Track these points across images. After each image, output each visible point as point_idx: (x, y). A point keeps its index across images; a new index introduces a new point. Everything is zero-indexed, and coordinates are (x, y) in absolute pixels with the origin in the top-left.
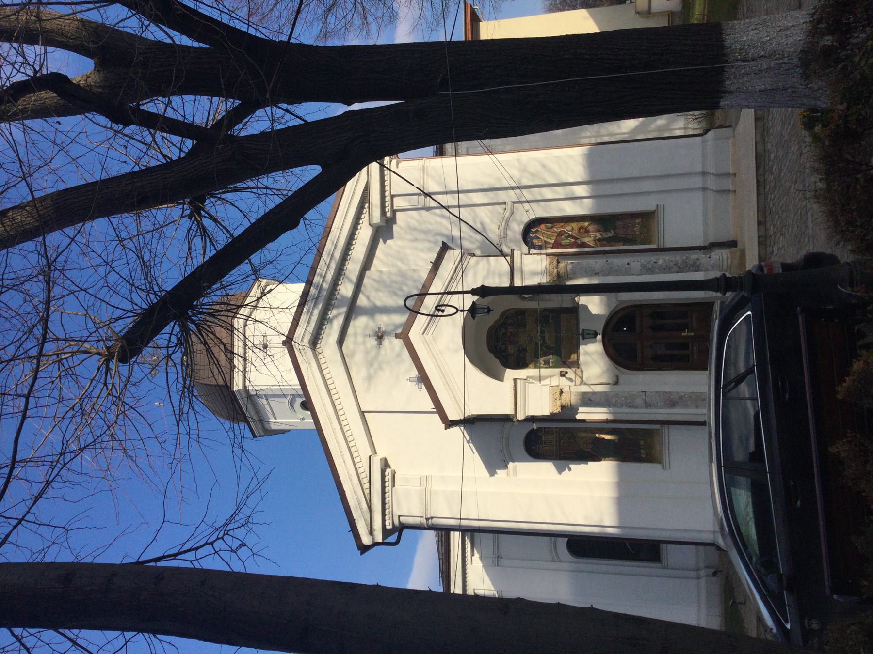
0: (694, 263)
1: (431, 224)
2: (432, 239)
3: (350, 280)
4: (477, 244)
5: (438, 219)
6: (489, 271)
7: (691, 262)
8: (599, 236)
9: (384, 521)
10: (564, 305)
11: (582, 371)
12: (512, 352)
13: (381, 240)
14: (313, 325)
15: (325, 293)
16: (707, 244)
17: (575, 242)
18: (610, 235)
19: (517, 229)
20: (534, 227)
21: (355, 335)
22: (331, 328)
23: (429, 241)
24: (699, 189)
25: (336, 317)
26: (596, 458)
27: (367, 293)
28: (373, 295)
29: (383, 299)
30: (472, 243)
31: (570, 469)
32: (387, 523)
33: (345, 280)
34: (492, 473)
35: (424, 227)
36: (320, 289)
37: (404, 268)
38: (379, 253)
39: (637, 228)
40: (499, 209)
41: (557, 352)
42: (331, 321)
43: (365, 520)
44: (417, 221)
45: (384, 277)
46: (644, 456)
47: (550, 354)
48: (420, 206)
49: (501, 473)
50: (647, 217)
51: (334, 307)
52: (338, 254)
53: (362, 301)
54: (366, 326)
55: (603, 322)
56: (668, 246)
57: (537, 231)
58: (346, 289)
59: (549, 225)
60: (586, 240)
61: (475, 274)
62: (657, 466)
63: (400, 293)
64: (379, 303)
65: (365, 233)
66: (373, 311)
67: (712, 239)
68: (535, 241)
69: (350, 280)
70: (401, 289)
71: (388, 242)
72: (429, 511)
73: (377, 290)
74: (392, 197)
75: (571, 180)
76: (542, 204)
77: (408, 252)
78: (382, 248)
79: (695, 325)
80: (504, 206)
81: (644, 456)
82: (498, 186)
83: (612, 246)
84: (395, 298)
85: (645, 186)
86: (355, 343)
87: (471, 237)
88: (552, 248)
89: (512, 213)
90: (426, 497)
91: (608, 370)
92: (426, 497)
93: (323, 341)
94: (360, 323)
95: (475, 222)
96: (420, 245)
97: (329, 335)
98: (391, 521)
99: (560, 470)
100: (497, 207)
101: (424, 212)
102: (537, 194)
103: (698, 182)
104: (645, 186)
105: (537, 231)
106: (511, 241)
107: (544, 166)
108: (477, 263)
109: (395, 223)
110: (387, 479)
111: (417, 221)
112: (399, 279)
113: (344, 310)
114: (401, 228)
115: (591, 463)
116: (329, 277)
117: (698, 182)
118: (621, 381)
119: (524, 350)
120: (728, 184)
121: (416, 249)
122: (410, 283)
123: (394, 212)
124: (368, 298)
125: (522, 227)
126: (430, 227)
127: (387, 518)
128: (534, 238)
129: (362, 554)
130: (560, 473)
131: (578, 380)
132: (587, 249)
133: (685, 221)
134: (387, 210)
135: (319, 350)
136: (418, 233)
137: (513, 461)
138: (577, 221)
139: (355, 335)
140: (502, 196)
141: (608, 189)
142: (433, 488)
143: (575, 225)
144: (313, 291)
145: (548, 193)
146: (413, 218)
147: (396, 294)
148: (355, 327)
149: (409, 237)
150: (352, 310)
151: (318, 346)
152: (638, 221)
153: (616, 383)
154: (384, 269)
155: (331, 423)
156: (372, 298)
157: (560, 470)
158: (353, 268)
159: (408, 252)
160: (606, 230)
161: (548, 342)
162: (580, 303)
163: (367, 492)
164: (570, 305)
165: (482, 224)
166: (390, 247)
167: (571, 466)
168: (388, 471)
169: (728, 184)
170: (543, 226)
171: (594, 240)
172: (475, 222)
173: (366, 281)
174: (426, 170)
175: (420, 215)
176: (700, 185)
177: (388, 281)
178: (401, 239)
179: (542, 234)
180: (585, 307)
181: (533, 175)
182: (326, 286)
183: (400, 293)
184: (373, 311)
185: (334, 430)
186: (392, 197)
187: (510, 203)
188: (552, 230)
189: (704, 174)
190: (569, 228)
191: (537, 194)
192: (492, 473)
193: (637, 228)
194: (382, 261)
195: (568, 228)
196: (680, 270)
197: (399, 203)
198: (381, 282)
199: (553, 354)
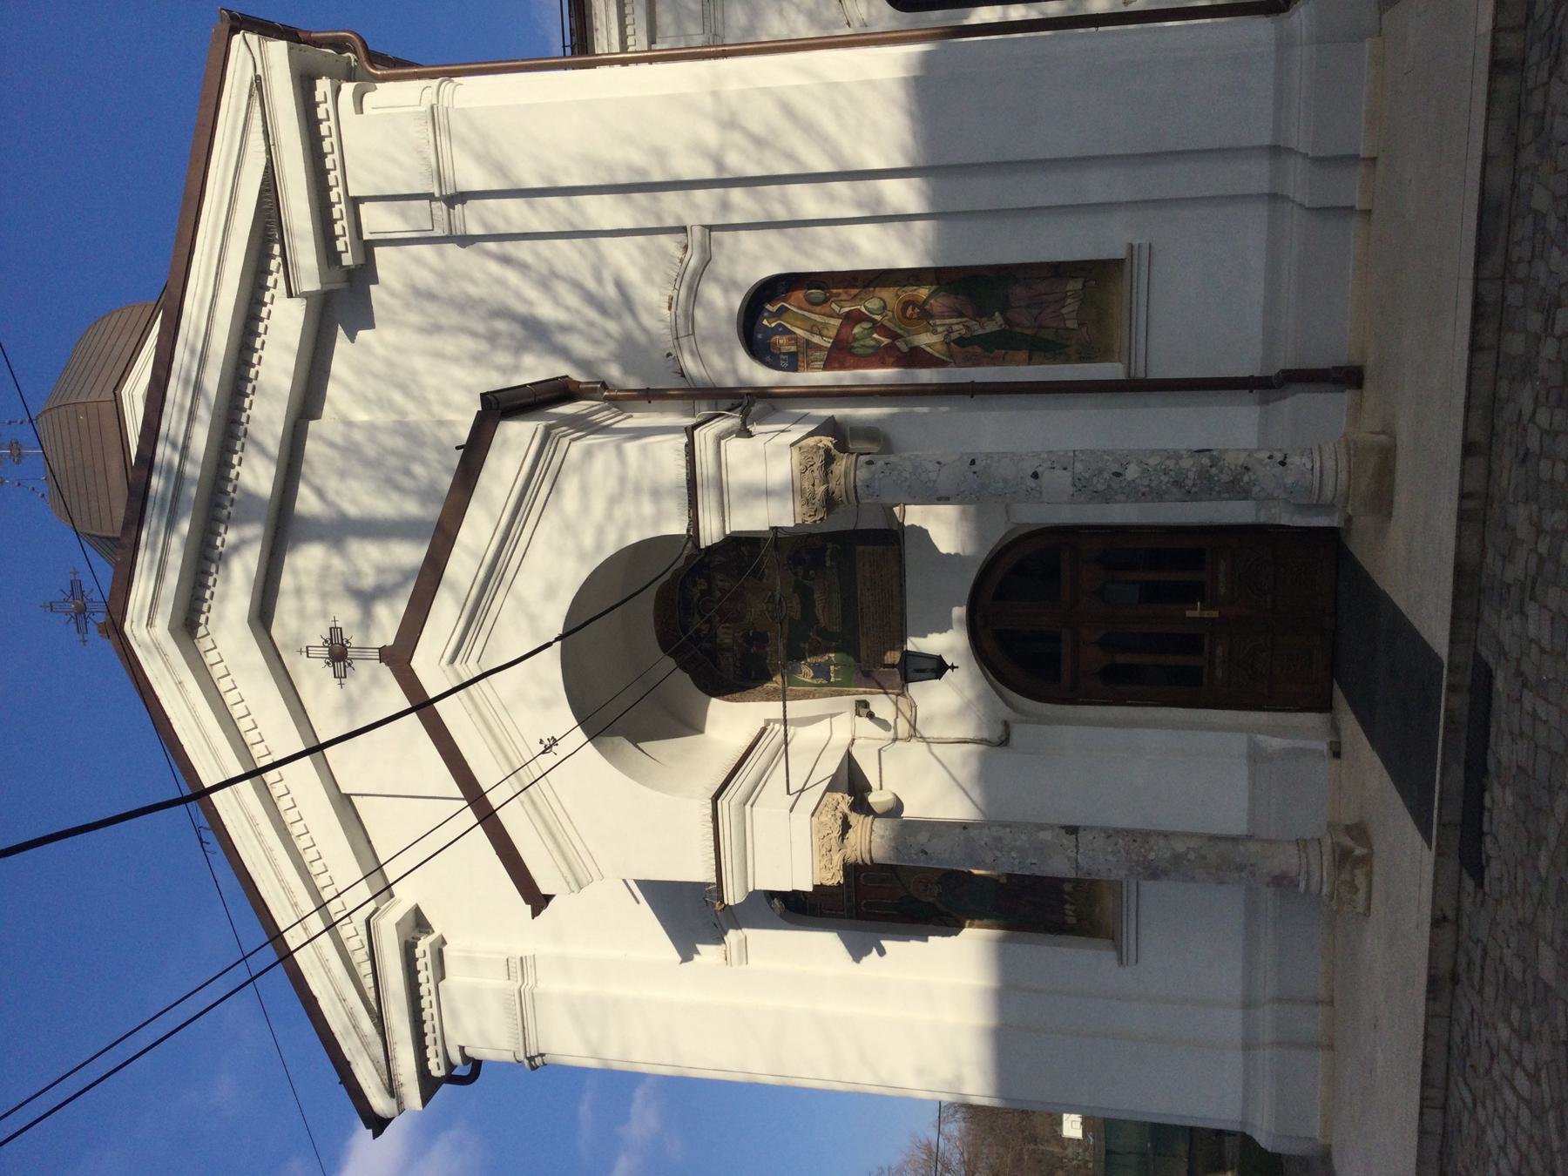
0: (1234, 482)
3: (262, 450)
4: (611, 346)
5: (494, 268)
6: (622, 480)
7: (1225, 478)
8: (959, 329)
9: (422, 1061)
10: (865, 525)
11: (913, 706)
13: (341, 331)
14: (172, 579)
16: (1273, 372)
18: (993, 325)
19: (722, 302)
21: (299, 592)
22: (227, 579)
23: (474, 334)
27: (317, 482)
29: (361, 498)
30: (596, 342)
31: (882, 952)
32: (432, 1065)
33: (249, 448)
34: (687, 954)
35: (454, 289)
36: (179, 479)
37: (415, 414)
38: (337, 366)
40: (669, 243)
41: (847, 644)
42: (223, 559)
43: (374, 1061)
44: (433, 270)
45: (358, 436)
46: (1072, 920)
47: (828, 650)
48: (438, 232)
49: (708, 954)
50: (1099, 275)
51: (229, 521)
52: (212, 380)
53: (307, 502)
54: (325, 570)
55: (972, 575)
56: (1156, 373)
57: (783, 310)
58: (256, 475)
59: (816, 293)
60: (925, 340)
61: (585, 490)
62: (1108, 957)
63: (406, 482)
64: (352, 510)
65: (285, 321)
66: (340, 530)
67: (1287, 359)
69: (262, 450)
70: (408, 473)
71: (362, 334)
72: (532, 1039)
73: (342, 475)
74: (354, 203)
76: (791, 231)
77: (420, 363)
78: (345, 354)
79: (1223, 590)
80: (681, 237)
81: (1072, 920)
82: (657, 176)
84: (395, 496)
85: (1096, 185)
86: (301, 614)
87: (591, 324)
88: (827, 366)
89: (706, 261)
90: (522, 1008)
91: (979, 697)
92: (522, 1008)
94: (306, 561)
95: (599, 280)
96: (450, 344)
97: (223, 598)
99: (858, 953)
101: (452, 249)
102: (775, 203)
103: (1257, 176)
104: (1096, 185)
105: (783, 310)
106: (705, 339)
107: (788, 111)
108: (588, 453)
109: (375, 281)
110: (420, 965)
111: (433, 270)
112: (399, 443)
113: (255, 531)
114: (392, 294)
116: (200, 440)
117: (1257, 176)
118: (1015, 737)
119: (761, 639)
120: (1350, 189)
121: (439, 355)
122: (431, 455)
124: (320, 493)
125: (737, 301)
126: (474, 291)
127: (430, 1053)
128: (775, 331)
129: (376, 1135)
131: (903, 728)
132: (926, 376)
133: (1208, 294)
134: (340, 246)
136: (444, 307)
137: (738, 927)
138: (896, 283)
140: (673, 206)
142: (542, 986)
143: (888, 294)
144: (157, 483)
145: (807, 200)
146: (419, 261)
147: (399, 489)
148: (295, 572)
149: (414, 318)
150: (283, 529)
151: (201, 631)
152: (1074, 285)
153: (1004, 741)
154: (361, 416)
155: (258, 835)
156: (331, 496)
157: (858, 953)
158: (267, 413)
159: (420, 363)
160: (981, 313)
161: (823, 621)
163: (371, 995)
164: (880, 525)
165: (620, 285)
166: (367, 349)
167: (884, 943)
168: (424, 945)
169: (1350, 189)
170: (799, 295)
173: (311, 446)
174: (442, 119)
175: (442, 256)
176: (1265, 188)
177: (371, 451)
178: (399, 324)
179: (797, 322)
180: (922, 534)
181: (759, 142)
182: (193, 470)
183: (406, 482)
184: (340, 530)
185: (268, 853)
186: (354, 203)
187: (697, 234)
188: (825, 309)
189: (1276, 151)
190: (874, 304)
191: (775, 203)
192: (687, 954)
193: (1071, 306)
194: (348, 387)
195: (871, 305)
197: (375, 220)
198: (350, 450)
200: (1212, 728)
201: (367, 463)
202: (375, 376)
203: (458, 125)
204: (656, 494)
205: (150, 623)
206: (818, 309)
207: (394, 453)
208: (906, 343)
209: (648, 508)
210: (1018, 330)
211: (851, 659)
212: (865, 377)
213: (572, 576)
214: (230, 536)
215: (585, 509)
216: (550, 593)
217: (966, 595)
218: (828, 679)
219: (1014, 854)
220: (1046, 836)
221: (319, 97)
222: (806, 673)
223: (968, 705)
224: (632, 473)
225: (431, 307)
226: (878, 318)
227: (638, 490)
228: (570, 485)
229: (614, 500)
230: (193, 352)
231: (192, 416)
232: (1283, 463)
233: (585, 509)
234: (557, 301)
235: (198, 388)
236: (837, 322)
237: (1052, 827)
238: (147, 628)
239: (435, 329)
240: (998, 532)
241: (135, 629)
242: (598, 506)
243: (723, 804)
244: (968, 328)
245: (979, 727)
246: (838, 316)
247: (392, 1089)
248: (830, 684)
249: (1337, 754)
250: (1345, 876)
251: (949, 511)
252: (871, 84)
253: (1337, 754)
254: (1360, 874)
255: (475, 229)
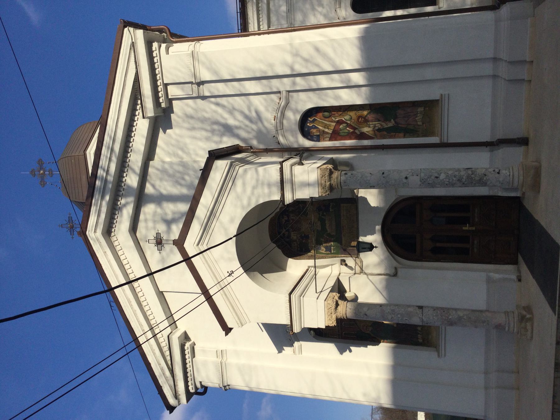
1: (206, 112)
2: (209, 128)
3: (134, 171)
4: (254, 134)
5: (213, 107)
6: (257, 180)
7: (477, 178)
8: (378, 125)
9: (187, 386)
11: (362, 262)
12: (295, 238)
13: (161, 130)
14: (103, 216)
15: (110, 186)
16: (494, 140)
17: (353, 133)
18: (391, 124)
19: (293, 117)
20: (310, 117)
21: (146, 220)
22: (122, 216)
23: (206, 130)
24: (489, 76)
25: (125, 205)
26: (375, 342)
27: (152, 182)
28: (158, 183)
29: (167, 187)
30: (248, 132)
31: (350, 351)
32: (190, 388)
33: (130, 171)
34: (280, 350)
35: (199, 115)
37: (186, 159)
38: (160, 142)
39: (419, 117)
41: (338, 240)
42: (120, 209)
44: (192, 108)
45: (167, 166)
46: (421, 341)
47: (331, 241)
48: (194, 95)
49: (287, 350)
50: (430, 106)
53: (149, 189)
54: (155, 213)
55: (383, 214)
56: (451, 141)
57: (315, 120)
58: (132, 180)
61: (244, 184)
63: (183, 182)
64: (164, 192)
65: (142, 127)
66: (160, 199)
67: (500, 135)
68: (314, 131)
69: (134, 171)
70: (183, 179)
71: (168, 131)
72: (225, 379)
74: (166, 85)
75: (348, 67)
77: (188, 141)
78: (162, 138)
79: (477, 220)
80: (279, 95)
81: (421, 341)
82: (270, 74)
83: (391, 137)
84: (179, 187)
85: (429, 73)
86: (147, 228)
87: (247, 126)
89: (287, 103)
92: (222, 368)
93: (116, 229)
94: (148, 210)
95: (250, 111)
96: (198, 134)
97: (120, 222)
98: (193, 386)
99: (342, 351)
100: (273, 96)
101: (199, 101)
102: (312, 82)
103: (488, 69)
104: (429, 73)
105: (315, 120)
107: (317, 50)
109: (173, 112)
111: (192, 108)
112: (180, 169)
113: (131, 199)
114: (178, 117)
115: (370, 347)
116: (113, 168)
117: (488, 69)
119: (307, 237)
121: (194, 138)
122: (191, 173)
123: (170, 101)
124: (153, 186)
125: (298, 117)
126: (206, 115)
127: (190, 384)
128: (312, 128)
129: (170, 413)
130: (341, 353)
131: (358, 269)
132: (366, 142)
133: (470, 112)
134: (161, 100)
135: (114, 239)
136: (196, 121)
137: (298, 341)
138: (356, 110)
139: (146, 220)
140: (276, 84)
141: (388, 76)
142: (229, 361)
143: (352, 114)
144: (98, 183)
145: (324, 81)
147: (181, 185)
148: (145, 214)
149: (186, 125)
150: (141, 197)
151: (113, 234)
152: (421, 109)
153: (395, 275)
154: (168, 159)
156: (157, 187)
157: (342, 351)
158: (136, 159)
159: (188, 141)
160: (386, 120)
161: (329, 231)
162: (359, 196)
163: (169, 363)
164: (350, 196)
165: (257, 112)
166: (170, 136)
167: (351, 348)
168: (188, 345)
170: (320, 115)
171: (374, 131)
172: (250, 111)
173: (150, 170)
174: (195, 55)
175: (195, 103)
176: (491, 73)
177: (171, 171)
178: (181, 127)
180: (365, 199)
181: (306, 60)
182: (110, 178)
183: (183, 182)
184: (160, 199)
186: (166, 85)
187: (284, 93)
189: (495, 60)
190: (347, 117)
191: (312, 82)
192: (280, 350)
193: (419, 117)
194: (163, 149)
195: (346, 117)
196: (464, 185)
197: (173, 91)
198: (164, 171)
199: (333, 241)
200: (429, 268)
201: (170, 176)
202: (173, 145)
203: (201, 58)
204: (269, 185)
205: (95, 232)
206: (327, 119)
207: (179, 172)
208: (359, 131)
209: (266, 190)
210: (400, 125)
211: (339, 245)
212: (344, 143)
213: (240, 215)
214: (123, 201)
215: (244, 191)
216: (232, 221)
217: (381, 221)
218: (331, 251)
219: (399, 316)
220: (410, 309)
221: (154, 49)
222: (323, 249)
223: (382, 261)
224: (261, 177)
225: (192, 121)
226: (349, 122)
227: (263, 184)
228: (239, 183)
229: (254, 188)
230: (110, 137)
231: (110, 160)
232: (498, 173)
233: (244, 191)
234: (235, 119)
235: (112, 150)
236: (334, 124)
237: (413, 306)
238: (94, 234)
239: (193, 129)
240: (392, 199)
241: (90, 233)
242: (249, 190)
243: (293, 296)
244: (381, 125)
245: (386, 269)
246: (334, 122)
247: (176, 396)
248: (331, 254)
249: (520, 280)
250: (523, 325)
251: (374, 191)
252: (347, 39)
253: (520, 280)
254: (529, 325)
255: (207, 94)
